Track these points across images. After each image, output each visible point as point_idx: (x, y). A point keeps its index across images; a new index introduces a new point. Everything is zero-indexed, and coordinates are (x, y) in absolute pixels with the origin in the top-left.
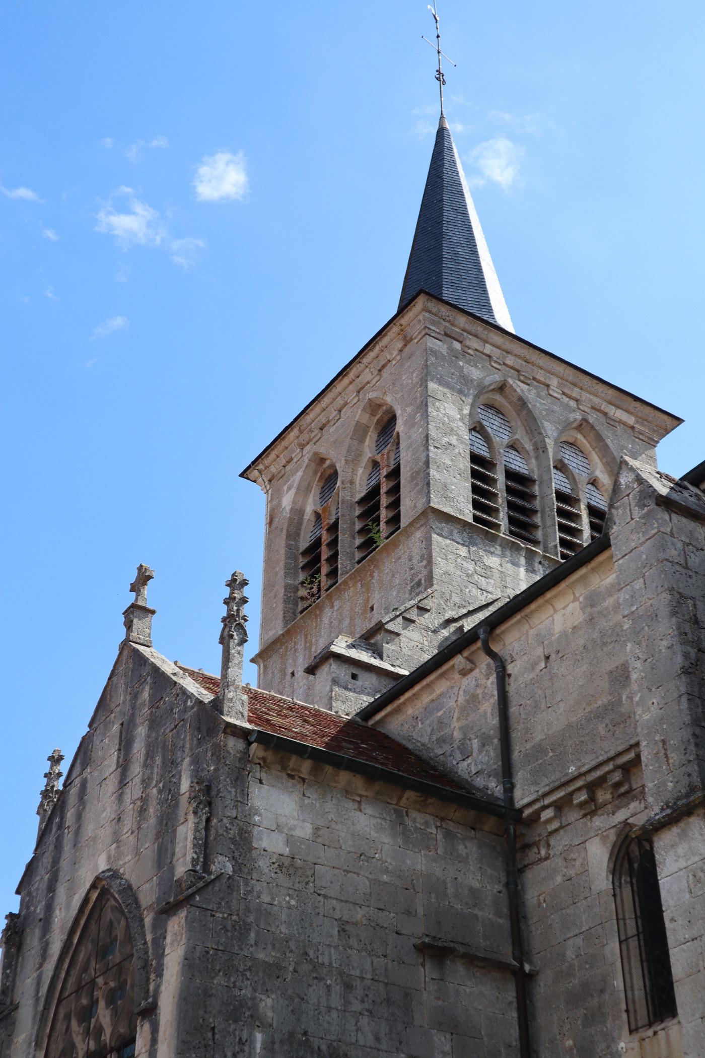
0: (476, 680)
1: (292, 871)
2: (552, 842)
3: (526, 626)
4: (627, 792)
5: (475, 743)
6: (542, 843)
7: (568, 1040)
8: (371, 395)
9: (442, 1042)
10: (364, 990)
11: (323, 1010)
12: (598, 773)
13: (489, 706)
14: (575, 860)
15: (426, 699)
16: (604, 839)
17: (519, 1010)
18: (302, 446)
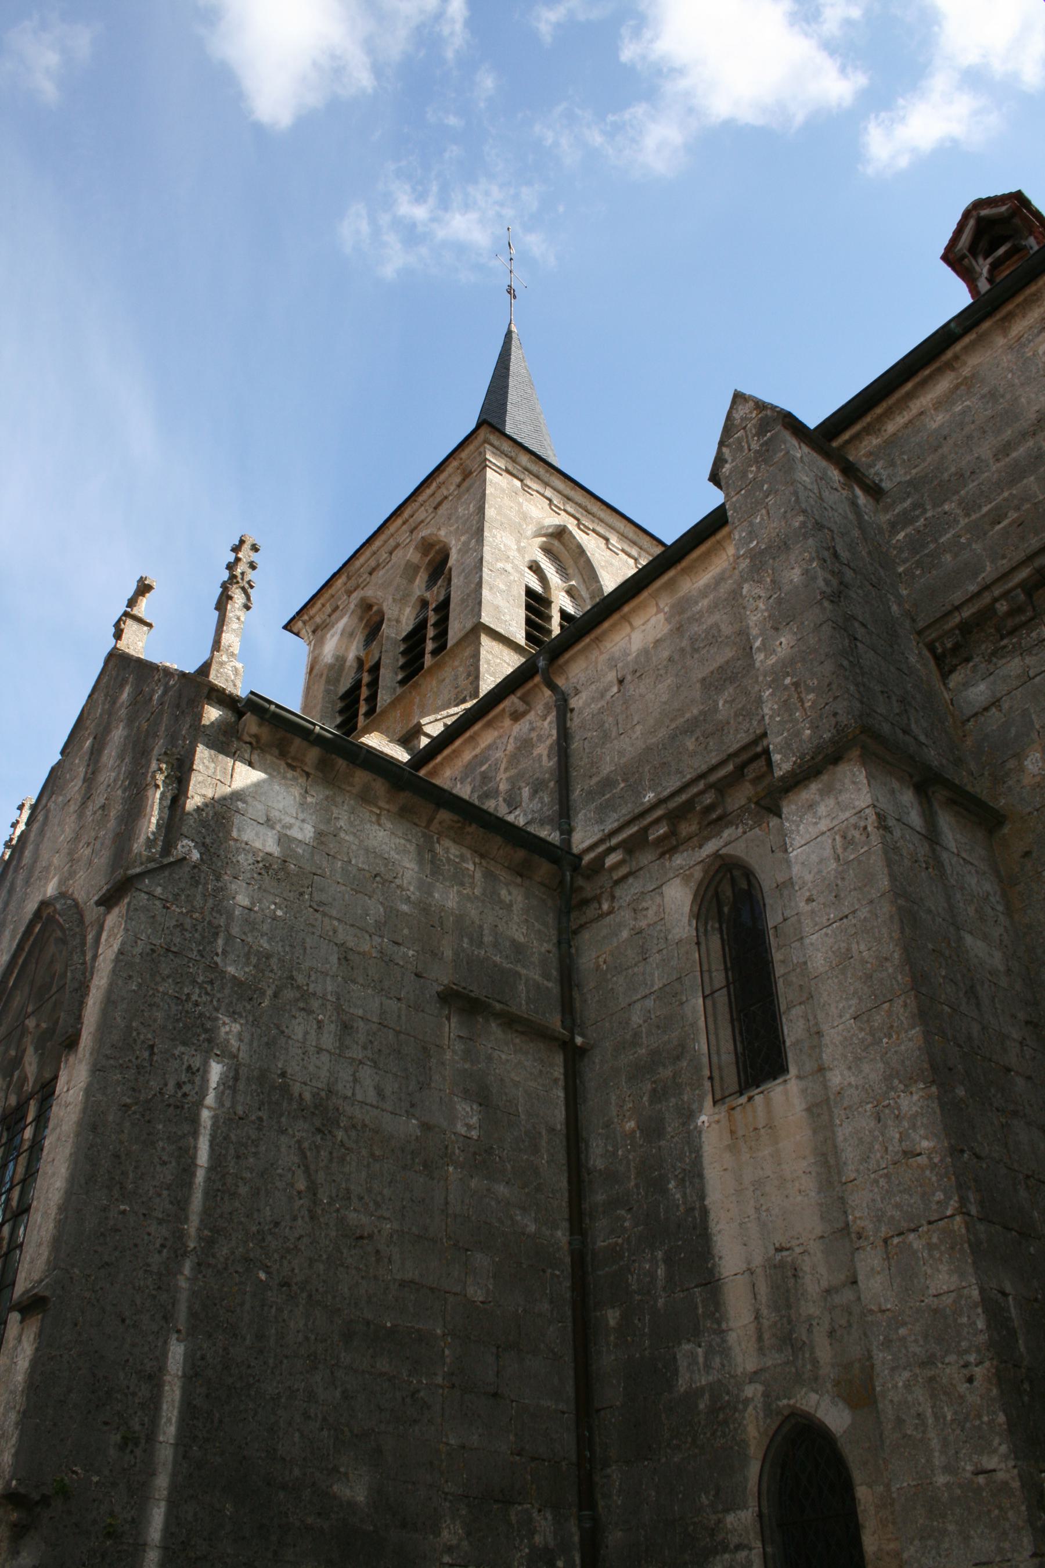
0: (530, 723)
1: (281, 875)
2: (618, 893)
3: (596, 653)
4: (720, 818)
5: (526, 792)
6: (605, 896)
7: (629, 1121)
8: (424, 532)
9: (467, 1113)
10: (368, 1035)
11: (312, 1050)
12: (684, 797)
13: (543, 752)
14: (647, 909)
15: (467, 756)
16: (687, 879)
17: (566, 1089)
18: (349, 593)
